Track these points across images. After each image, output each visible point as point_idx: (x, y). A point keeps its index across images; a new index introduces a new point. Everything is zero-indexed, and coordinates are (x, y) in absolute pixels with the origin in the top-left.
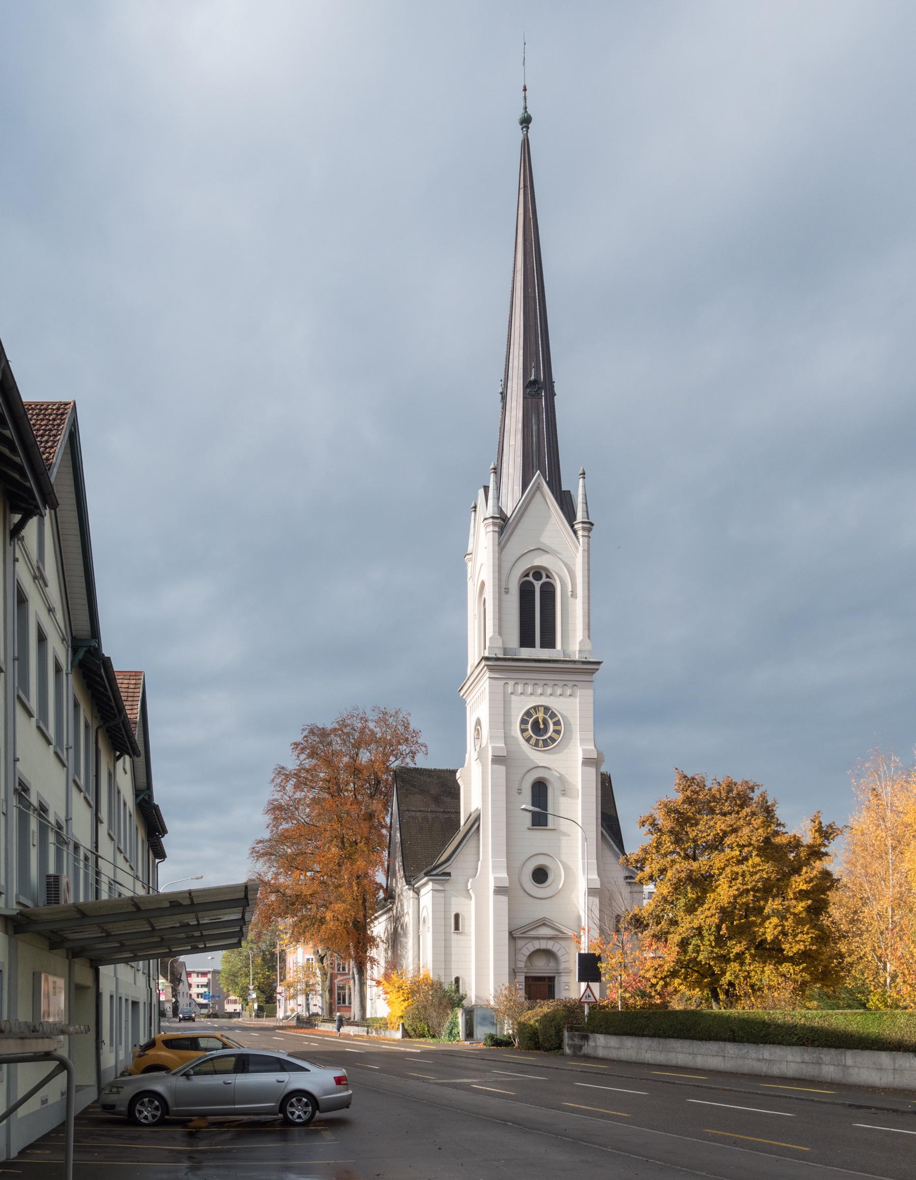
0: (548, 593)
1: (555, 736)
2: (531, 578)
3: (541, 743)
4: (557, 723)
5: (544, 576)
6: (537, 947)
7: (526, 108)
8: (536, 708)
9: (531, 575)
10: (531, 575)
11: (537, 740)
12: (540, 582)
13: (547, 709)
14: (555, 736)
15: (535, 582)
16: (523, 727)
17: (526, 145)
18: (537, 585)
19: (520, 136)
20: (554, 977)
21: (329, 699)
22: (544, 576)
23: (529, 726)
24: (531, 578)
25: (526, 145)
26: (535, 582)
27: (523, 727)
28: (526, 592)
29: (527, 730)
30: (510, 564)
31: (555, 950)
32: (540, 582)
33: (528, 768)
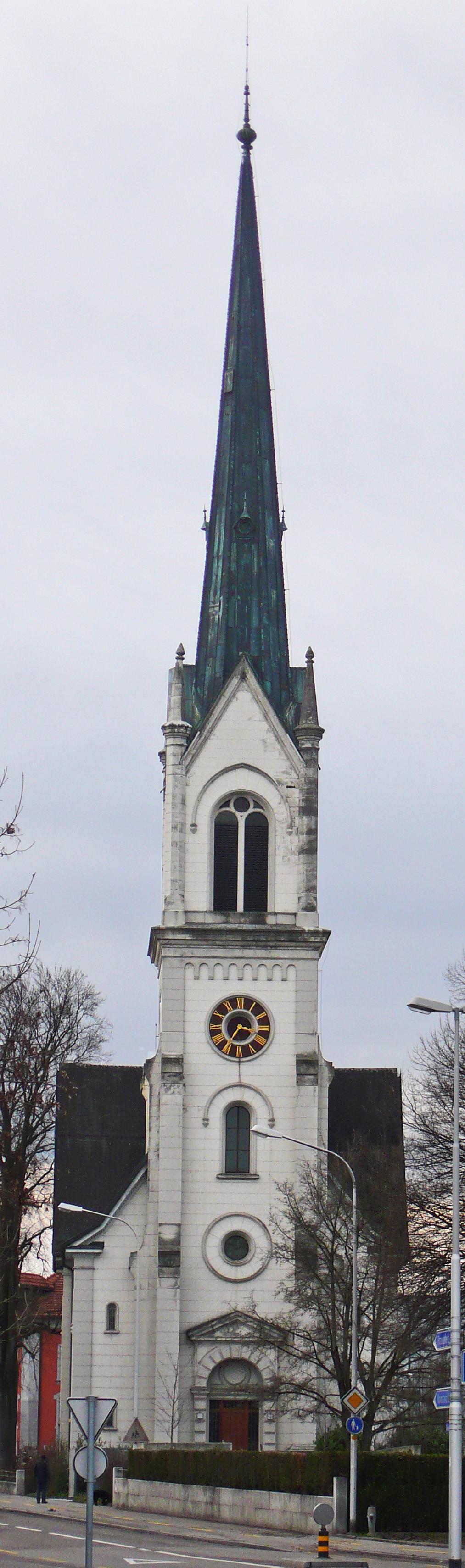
0: (259, 830)
1: (261, 1040)
2: (232, 809)
3: (239, 1051)
4: (265, 1021)
5: (252, 805)
6: (227, 1355)
7: (247, 119)
8: (233, 1001)
9: (232, 804)
10: (232, 804)
11: (234, 1048)
12: (246, 814)
13: (248, 1001)
14: (261, 1040)
15: (238, 814)
16: (213, 1027)
17: (247, 105)
18: (241, 818)
19: (239, 161)
20: (210, 1441)
21: (107, 1303)
22: (252, 805)
23: (225, 1018)
24: (232, 809)
25: (247, 105)
26: (238, 814)
27: (213, 1027)
28: (224, 832)
29: (220, 1031)
30: (202, 1230)
31: (253, 1360)
32: (246, 814)
33: (218, 1088)
